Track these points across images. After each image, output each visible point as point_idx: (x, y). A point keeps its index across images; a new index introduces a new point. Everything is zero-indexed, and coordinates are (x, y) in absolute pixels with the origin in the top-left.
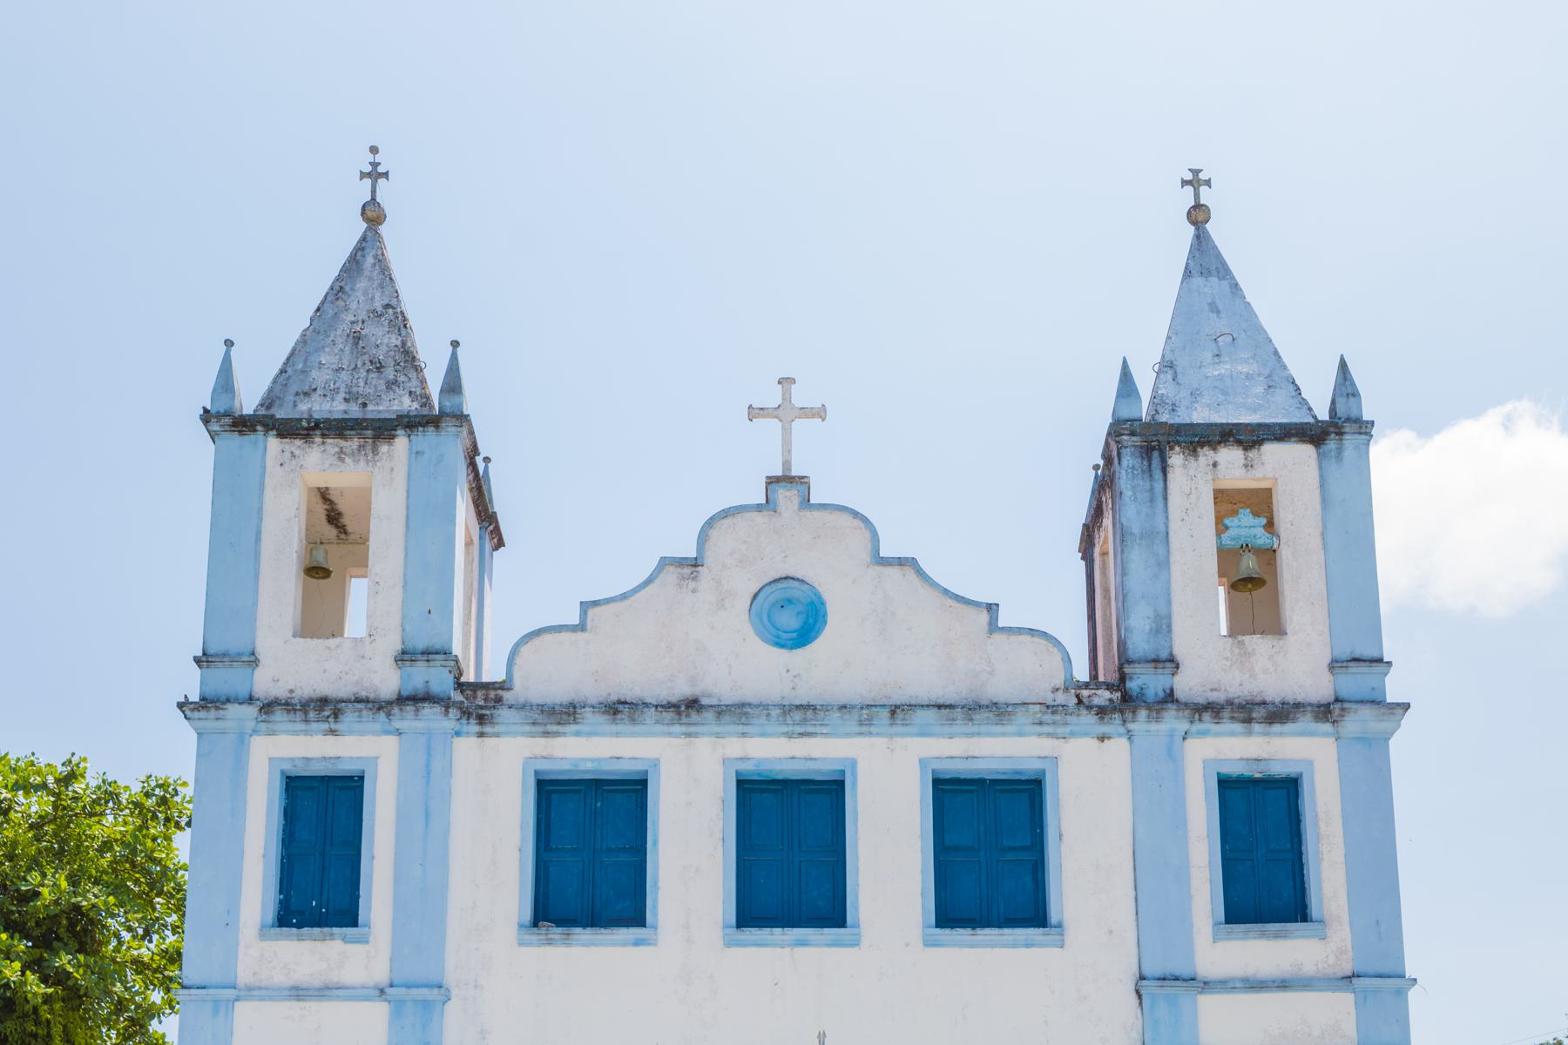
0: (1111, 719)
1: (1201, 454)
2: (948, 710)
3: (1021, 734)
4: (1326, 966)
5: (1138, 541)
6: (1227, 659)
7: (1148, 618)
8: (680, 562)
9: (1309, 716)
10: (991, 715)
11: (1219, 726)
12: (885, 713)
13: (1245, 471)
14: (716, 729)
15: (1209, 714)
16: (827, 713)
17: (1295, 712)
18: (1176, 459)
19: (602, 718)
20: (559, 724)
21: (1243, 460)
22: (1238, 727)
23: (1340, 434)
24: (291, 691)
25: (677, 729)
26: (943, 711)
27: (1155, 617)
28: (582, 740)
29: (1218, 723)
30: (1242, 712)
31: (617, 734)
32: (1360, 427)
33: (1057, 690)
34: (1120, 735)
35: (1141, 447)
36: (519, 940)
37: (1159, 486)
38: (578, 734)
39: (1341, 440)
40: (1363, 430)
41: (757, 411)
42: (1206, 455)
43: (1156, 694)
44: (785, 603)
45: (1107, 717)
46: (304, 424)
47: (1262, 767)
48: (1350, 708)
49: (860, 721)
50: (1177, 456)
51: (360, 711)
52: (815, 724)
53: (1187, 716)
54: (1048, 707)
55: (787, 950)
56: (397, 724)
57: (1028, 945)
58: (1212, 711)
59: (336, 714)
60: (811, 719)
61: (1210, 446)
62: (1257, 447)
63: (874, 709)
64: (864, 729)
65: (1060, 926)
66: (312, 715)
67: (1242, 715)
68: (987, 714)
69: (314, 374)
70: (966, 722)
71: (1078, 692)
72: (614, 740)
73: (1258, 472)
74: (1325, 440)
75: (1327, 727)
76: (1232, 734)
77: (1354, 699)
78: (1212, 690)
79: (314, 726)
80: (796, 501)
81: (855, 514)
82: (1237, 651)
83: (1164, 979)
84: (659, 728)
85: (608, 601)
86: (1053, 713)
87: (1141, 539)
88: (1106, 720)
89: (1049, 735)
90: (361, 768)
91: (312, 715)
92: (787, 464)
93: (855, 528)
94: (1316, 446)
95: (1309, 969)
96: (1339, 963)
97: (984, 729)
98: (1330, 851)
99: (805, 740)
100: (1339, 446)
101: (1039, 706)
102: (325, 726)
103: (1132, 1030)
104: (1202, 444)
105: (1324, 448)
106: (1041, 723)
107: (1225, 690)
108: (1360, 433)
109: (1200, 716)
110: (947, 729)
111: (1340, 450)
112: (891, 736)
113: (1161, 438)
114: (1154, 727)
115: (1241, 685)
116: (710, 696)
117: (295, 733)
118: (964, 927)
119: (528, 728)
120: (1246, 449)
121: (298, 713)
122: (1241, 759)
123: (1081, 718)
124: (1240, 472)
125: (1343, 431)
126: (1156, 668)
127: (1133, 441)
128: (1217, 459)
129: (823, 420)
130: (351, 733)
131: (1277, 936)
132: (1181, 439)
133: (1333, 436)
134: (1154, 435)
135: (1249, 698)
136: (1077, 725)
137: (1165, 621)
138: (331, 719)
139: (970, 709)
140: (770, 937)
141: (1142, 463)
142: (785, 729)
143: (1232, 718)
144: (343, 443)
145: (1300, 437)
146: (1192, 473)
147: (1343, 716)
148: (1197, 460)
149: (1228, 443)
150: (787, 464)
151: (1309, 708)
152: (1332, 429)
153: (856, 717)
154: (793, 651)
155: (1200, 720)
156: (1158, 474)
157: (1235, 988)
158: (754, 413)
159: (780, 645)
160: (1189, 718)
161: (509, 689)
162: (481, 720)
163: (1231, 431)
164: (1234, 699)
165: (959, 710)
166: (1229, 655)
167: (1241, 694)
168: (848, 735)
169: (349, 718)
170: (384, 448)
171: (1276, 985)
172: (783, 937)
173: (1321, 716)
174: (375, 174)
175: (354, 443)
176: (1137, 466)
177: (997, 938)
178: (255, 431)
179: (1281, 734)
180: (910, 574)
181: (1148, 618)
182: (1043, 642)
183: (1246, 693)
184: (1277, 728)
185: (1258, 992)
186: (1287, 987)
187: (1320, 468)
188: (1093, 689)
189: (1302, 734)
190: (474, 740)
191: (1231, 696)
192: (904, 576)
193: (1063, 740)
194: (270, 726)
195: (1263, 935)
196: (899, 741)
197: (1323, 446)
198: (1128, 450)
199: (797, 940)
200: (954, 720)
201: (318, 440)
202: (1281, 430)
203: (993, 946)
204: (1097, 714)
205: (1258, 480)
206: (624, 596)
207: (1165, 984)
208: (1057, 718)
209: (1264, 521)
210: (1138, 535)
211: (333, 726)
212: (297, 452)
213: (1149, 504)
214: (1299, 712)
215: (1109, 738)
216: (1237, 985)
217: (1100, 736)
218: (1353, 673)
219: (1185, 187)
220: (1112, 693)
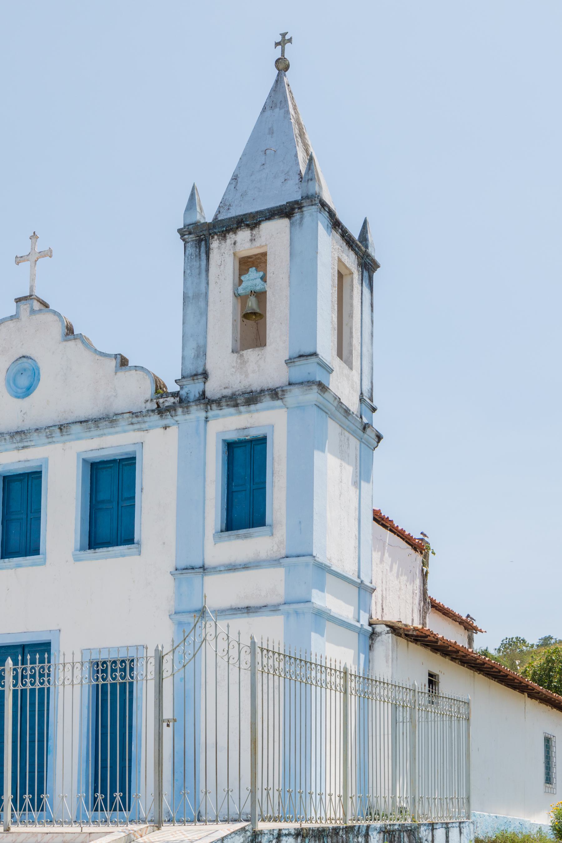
0: (166, 415)
1: (228, 238)
2: (85, 423)
3: (125, 431)
4: (272, 552)
5: (191, 301)
6: (233, 367)
7: (193, 349)
9: (268, 398)
10: (107, 423)
11: (222, 411)
12: (57, 430)
13: (250, 243)
15: (215, 404)
16: (31, 434)
17: (260, 397)
18: (215, 244)
21: (250, 237)
22: (232, 410)
23: (300, 208)
26: (83, 424)
27: (197, 347)
29: (221, 409)
30: (231, 401)
32: (312, 201)
33: (147, 401)
34: (174, 424)
35: (196, 240)
36: (74, 558)
37: (204, 263)
39: (302, 212)
40: (314, 203)
41: (19, 259)
42: (231, 237)
43: (195, 396)
44: (22, 372)
45: (164, 415)
47: (246, 432)
48: (286, 390)
49: (47, 436)
50: (216, 242)
52: (27, 441)
53: (202, 408)
54: (133, 414)
55: (14, 570)
57: (123, 556)
58: (216, 403)
60: (25, 439)
61: (233, 231)
62: (258, 226)
63: (51, 428)
64: (50, 440)
65: (138, 543)
67: (232, 403)
68: (105, 423)
70: (96, 428)
71: (158, 400)
72: (124, 435)
73: (257, 243)
74: (293, 214)
75: (278, 403)
76: (231, 415)
77: (298, 382)
78: (225, 388)
80: (28, 310)
82: (239, 361)
83: (187, 569)
86: (137, 416)
87: (193, 299)
88: (163, 417)
89: (140, 430)
90: (221, 440)
93: (55, 321)
94: (289, 218)
95: (263, 555)
96: (279, 549)
97: (106, 431)
98: (279, 481)
99: (26, 450)
100: (301, 216)
101: (129, 414)
103: (171, 600)
104: (228, 231)
105: (294, 219)
106: (132, 424)
107: (232, 387)
108: (312, 205)
109: (211, 406)
110: (88, 434)
111: (302, 218)
112: (64, 442)
113: (204, 233)
114: (187, 417)
115: (240, 382)
118: (102, 547)
120: (252, 229)
122: (237, 429)
123: (151, 417)
124: (248, 245)
125: (302, 205)
126: (193, 380)
127: (191, 238)
128: (236, 239)
131: (246, 537)
132: (216, 231)
133: (296, 210)
134: (201, 231)
135: (244, 390)
136: (150, 422)
137: (202, 349)
139: (95, 421)
140: (4, 564)
141: (196, 251)
143: (228, 405)
145: (279, 215)
146: (223, 251)
147: (284, 395)
148: (225, 242)
149: (242, 228)
151: (267, 393)
152: (296, 206)
153: (45, 434)
154: (24, 399)
155: (211, 409)
156: (203, 256)
157: (221, 571)
159: (18, 397)
160: (203, 409)
163: (242, 219)
164: (236, 392)
165: (90, 422)
166: (235, 365)
167: (240, 388)
168: (44, 444)
171: (241, 567)
172: (9, 564)
173: (274, 396)
176: (193, 253)
177: (106, 553)
179: (257, 411)
181: (193, 349)
182: (142, 373)
183: (243, 387)
184: (253, 407)
185: (234, 572)
186: (248, 567)
187: (291, 230)
188: (165, 398)
189: (268, 408)
191: (234, 390)
192: (76, 345)
193: (146, 431)
195: (238, 537)
196: (68, 444)
197: (292, 218)
198: (189, 244)
199: (17, 564)
200: (90, 428)
202: (269, 213)
203: (106, 558)
204: (159, 414)
205: (258, 247)
207: (183, 572)
208: (140, 419)
209: (261, 274)
210: (191, 297)
213: (198, 276)
214: (262, 396)
215: (169, 427)
216: (222, 569)
217: (164, 426)
218: (299, 365)
219: (277, 47)
220: (174, 398)
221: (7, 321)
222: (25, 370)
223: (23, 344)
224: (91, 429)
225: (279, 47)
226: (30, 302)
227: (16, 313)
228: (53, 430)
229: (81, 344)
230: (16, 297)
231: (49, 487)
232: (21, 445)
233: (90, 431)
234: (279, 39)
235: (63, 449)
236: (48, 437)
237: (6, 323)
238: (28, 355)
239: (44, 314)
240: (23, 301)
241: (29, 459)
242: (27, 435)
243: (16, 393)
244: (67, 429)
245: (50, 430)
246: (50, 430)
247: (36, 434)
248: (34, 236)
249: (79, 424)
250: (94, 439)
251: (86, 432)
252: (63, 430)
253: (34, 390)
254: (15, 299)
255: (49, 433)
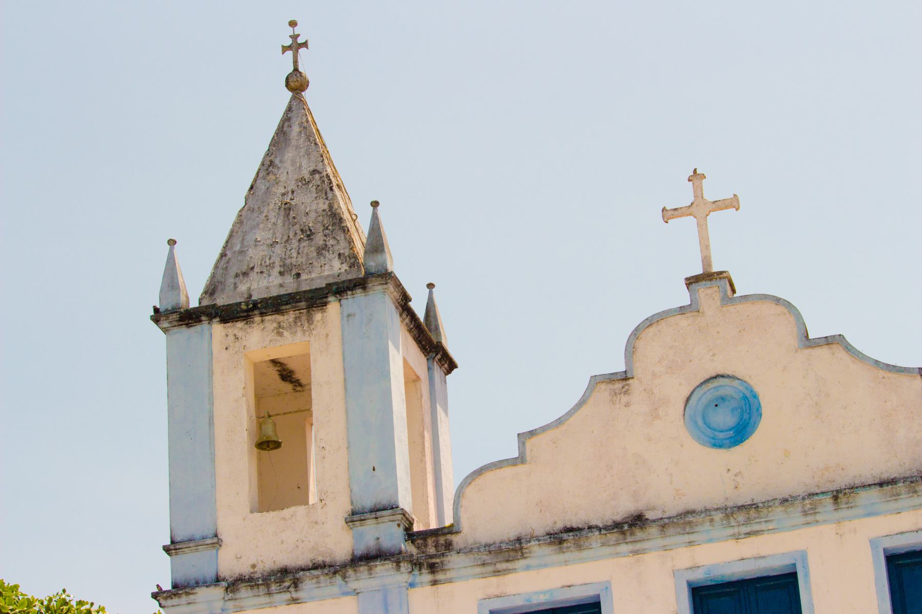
8: (611, 379)
14: (661, 542)
19: (548, 550)
20: (508, 561)
24: (254, 566)
25: (624, 548)
26: (885, 488)
28: (532, 573)
31: (566, 563)
38: (528, 568)
46: (244, 307)
51: (318, 577)
56: (353, 585)
59: (296, 584)
60: (755, 518)
63: (816, 498)
66: (274, 587)
69: (251, 252)
79: (277, 597)
81: (777, 300)
84: (606, 550)
85: (544, 429)
91: (274, 587)
92: (706, 261)
99: (753, 539)
102: (287, 596)
110: (893, 505)
116: (654, 509)
117: (261, 607)
119: (478, 570)
121: (261, 588)
129: (737, 209)
130: (312, 599)
138: (292, 589)
139: (912, 482)
142: (730, 531)
143: (603, 545)
144: (279, 318)
150: (706, 261)
153: (800, 509)
158: (668, 214)
161: (458, 532)
162: (433, 568)
168: (794, 527)
169: (308, 585)
170: (318, 316)
174: (296, 46)
175: (290, 316)
178: (200, 321)
180: (840, 353)
190: (429, 589)
194: (237, 603)
196: (847, 525)
200: (898, 495)
201: (257, 319)
206: (559, 422)
211: (295, 595)
212: (240, 334)
221: (674, 316)
222: (723, 399)
223: (714, 355)
224: (901, 497)
225: (290, 54)
226: (719, 283)
227: (691, 301)
228: (820, 500)
229: (844, 352)
230: (689, 275)
231: (815, 602)
232: (744, 529)
233: (896, 499)
234: (289, 42)
235: (837, 534)
236: (805, 513)
237: (672, 320)
238: (730, 373)
239: (753, 303)
240: (703, 283)
241: (763, 554)
242: (761, 511)
243: (713, 438)
244: (848, 498)
245: (813, 501)
246: (813, 501)
247: (781, 509)
248: (696, 177)
249: (878, 488)
250: (902, 514)
251: (888, 501)
252: (839, 500)
253: (752, 433)
254: (687, 279)
255: (808, 506)
